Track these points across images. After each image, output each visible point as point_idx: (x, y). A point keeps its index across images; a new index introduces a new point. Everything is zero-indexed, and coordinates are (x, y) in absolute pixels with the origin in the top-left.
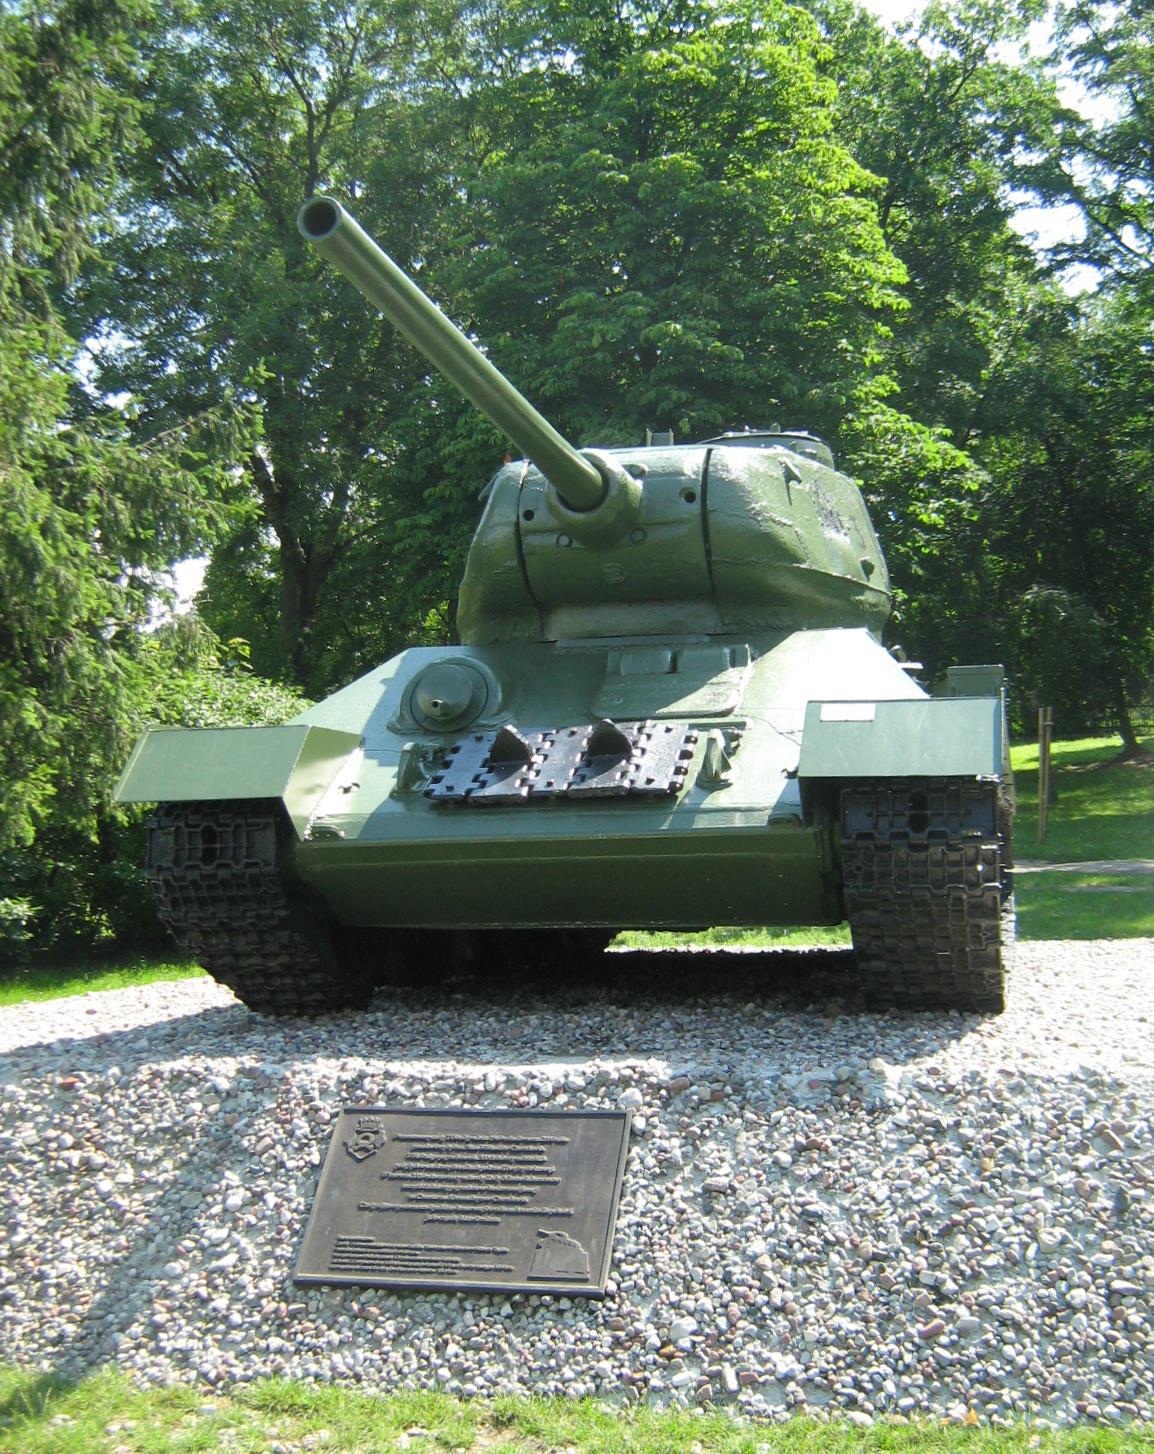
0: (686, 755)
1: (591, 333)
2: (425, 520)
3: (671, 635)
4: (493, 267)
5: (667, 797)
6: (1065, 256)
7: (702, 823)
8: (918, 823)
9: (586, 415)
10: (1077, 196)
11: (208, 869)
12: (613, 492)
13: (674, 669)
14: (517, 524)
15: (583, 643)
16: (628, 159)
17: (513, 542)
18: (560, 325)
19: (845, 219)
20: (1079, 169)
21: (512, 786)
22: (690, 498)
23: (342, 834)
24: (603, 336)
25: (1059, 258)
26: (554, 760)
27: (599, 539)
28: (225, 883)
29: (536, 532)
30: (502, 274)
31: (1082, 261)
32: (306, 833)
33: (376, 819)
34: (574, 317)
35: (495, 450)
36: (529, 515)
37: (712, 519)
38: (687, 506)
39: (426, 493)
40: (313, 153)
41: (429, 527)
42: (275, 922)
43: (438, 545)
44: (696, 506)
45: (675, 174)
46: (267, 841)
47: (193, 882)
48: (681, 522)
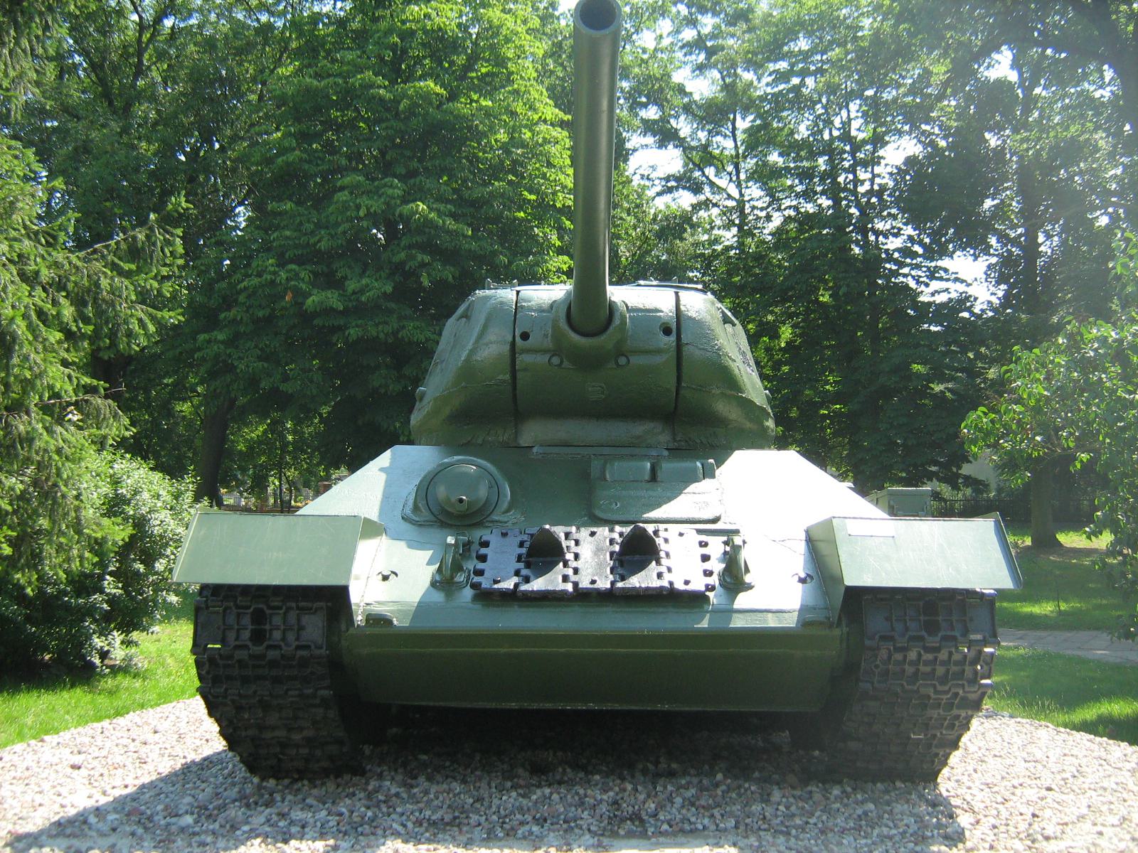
0: (705, 558)
1: (358, 207)
2: (221, 337)
3: (632, 448)
4: (283, 151)
5: (696, 600)
6: (673, 183)
7: (738, 622)
8: (932, 628)
9: (350, 267)
10: (681, 143)
11: (258, 650)
12: (617, 322)
13: (654, 478)
14: (513, 344)
15: (556, 450)
16: (393, 82)
17: (508, 360)
18: (335, 198)
19: (546, 141)
20: (684, 126)
21: (550, 582)
22: (667, 331)
23: (395, 622)
24: (368, 209)
25: (669, 185)
26: (589, 557)
27: (588, 363)
28: (273, 664)
29: (528, 351)
30: (291, 157)
31: (684, 188)
32: (359, 619)
33: (422, 608)
34: (346, 192)
35: (280, 288)
36: (525, 336)
37: (686, 350)
38: (666, 339)
39: (222, 316)
40: (140, 54)
41: (222, 342)
42: (318, 701)
43: (230, 356)
44: (673, 338)
45: (426, 96)
46: (314, 627)
47: (239, 661)
48: (659, 351)
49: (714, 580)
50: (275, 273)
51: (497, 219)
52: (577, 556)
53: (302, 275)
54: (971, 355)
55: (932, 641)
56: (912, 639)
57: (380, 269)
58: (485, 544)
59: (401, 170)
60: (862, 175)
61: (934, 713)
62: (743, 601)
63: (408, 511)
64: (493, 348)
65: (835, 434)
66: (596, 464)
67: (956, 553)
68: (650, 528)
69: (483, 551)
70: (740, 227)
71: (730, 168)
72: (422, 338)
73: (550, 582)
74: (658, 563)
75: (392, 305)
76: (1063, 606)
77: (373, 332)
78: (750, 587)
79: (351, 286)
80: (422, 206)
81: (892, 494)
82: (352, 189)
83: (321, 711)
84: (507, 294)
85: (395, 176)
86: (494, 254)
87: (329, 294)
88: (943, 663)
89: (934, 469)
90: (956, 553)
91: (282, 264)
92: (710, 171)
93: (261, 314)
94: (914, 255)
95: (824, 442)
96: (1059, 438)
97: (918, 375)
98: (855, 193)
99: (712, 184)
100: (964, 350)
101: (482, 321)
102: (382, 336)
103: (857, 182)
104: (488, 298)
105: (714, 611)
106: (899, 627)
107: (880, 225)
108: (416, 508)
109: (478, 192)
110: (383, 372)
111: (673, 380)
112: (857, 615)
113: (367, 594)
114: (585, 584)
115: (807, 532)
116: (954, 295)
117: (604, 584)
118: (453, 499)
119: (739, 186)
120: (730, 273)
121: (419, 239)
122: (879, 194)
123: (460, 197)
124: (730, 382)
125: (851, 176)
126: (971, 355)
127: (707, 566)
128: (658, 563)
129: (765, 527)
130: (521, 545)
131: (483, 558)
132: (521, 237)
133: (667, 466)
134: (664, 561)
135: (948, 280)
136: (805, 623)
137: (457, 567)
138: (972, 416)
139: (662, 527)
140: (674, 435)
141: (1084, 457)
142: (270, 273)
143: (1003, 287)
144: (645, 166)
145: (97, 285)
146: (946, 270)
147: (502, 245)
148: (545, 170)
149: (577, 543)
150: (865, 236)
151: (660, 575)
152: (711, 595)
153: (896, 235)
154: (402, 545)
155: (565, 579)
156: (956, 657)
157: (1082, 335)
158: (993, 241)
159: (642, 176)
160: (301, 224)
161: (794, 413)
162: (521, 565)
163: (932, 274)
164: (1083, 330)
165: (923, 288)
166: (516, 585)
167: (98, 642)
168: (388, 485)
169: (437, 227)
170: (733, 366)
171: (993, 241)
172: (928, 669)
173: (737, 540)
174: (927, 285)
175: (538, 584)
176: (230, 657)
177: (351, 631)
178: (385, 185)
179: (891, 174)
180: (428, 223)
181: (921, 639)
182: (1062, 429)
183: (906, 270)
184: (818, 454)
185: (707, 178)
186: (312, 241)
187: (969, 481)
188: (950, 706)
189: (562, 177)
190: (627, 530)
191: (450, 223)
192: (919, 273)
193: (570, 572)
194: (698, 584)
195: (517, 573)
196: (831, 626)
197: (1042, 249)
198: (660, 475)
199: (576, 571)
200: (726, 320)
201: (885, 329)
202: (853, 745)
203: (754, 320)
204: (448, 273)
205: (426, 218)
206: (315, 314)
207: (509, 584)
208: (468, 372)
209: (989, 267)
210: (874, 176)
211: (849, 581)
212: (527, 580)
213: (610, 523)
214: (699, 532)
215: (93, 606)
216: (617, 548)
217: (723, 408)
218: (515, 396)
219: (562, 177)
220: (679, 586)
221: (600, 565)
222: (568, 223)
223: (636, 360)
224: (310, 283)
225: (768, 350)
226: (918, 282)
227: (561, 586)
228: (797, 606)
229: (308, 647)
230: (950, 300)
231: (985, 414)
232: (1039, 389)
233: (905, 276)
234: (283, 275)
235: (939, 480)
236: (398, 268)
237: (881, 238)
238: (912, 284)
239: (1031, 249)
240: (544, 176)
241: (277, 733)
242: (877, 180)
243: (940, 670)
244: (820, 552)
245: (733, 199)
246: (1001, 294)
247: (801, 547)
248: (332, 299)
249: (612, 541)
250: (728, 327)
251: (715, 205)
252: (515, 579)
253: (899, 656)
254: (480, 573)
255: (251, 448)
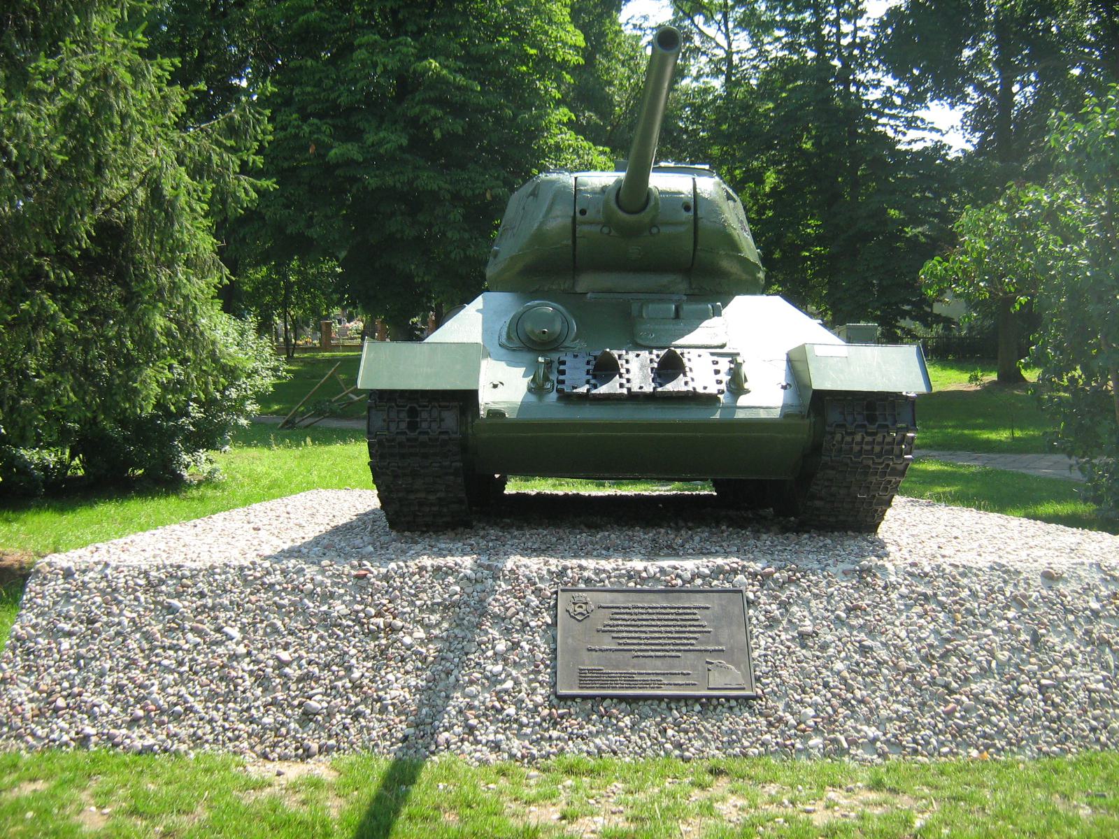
0: (717, 372)
1: (375, 65)
3: (660, 294)
5: (711, 400)
7: (740, 415)
8: (871, 419)
12: (652, 203)
15: (607, 295)
21: (611, 387)
22: (687, 208)
26: (637, 371)
27: (630, 232)
33: (524, 406)
34: (364, 51)
36: (583, 212)
37: (700, 223)
44: (691, 213)
48: (682, 224)
49: (723, 387)
50: (298, 127)
51: (501, 74)
52: (628, 371)
53: (324, 128)
54: (944, 201)
55: (872, 428)
56: (857, 426)
57: (395, 122)
58: (563, 363)
59: (411, 28)
60: (846, 27)
61: (873, 479)
62: (743, 401)
63: (504, 340)
64: (559, 220)
65: (815, 275)
66: (635, 307)
67: (891, 368)
68: (678, 351)
69: (562, 367)
70: (728, 79)
71: (719, 17)
72: (435, 187)
73: (611, 387)
74: (685, 375)
75: (407, 156)
76: (1018, 434)
77: (390, 181)
78: (748, 392)
79: (370, 138)
80: (434, 64)
81: (849, 328)
82: (371, 46)
83: (452, 478)
84: (568, 179)
85: (406, 34)
86: (502, 107)
87: (349, 146)
88: (879, 444)
89: (906, 308)
90: (891, 368)
91: (304, 118)
92: (699, 19)
93: (286, 165)
94: (892, 105)
95: (804, 282)
96: (1002, 283)
97: (894, 221)
98: (838, 44)
99: (701, 33)
100: (938, 196)
101: (548, 202)
102: (398, 185)
103: (840, 35)
104: (552, 182)
105: (724, 408)
106: (849, 418)
107: (861, 77)
108: (509, 338)
109: (484, 49)
110: (399, 218)
111: (691, 247)
112: (821, 409)
113: (488, 399)
114: (635, 389)
115: (788, 354)
116: (929, 144)
117: (649, 389)
118: (537, 332)
119: (727, 36)
120: (718, 122)
121: (432, 95)
122: (862, 46)
123: (468, 53)
124: (732, 244)
125: (834, 30)
126: (944, 201)
127: (719, 377)
128: (685, 375)
129: (759, 349)
130: (588, 363)
131: (563, 372)
132: (524, 90)
133: (687, 308)
134: (688, 374)
135: (924, 129)
136: (785, 415)
137: (546, 379)
138: (929, 264)
139: (686, 351)
140: (690, 284)
141: (1023, 299)
142: (294, 127)
143: (978, 134)
144: (637, 16)
145: (209, 159)
146: (923, 120)
147: (506, 98)
148: (547, 27)
149: (627, 362)
150: (847, 87)
151: (686, 383)
152: (721, 396)
153: (877, 83)
154: (503, 364)
155: (621, 386)
156: (888, 439)
157: (1019, 198)
158: (969, 90)
159: (635, 26)
160: (320, 80)
161: (777, 255)
162: (589, 377)
163: (911, 124)
164: (1020, 194)
165: (900, 137)
166: (588, 390)
167: (186, 458)
168: (484, 322)
169: (447, 82)
170: (735, 233)
171: (969, 90)
172: (869, 448)
173: (739, 360)
174: (904, 134)
175: (603, 389)
176: (393, 440)
177: (477, 421)
178: (399, 43)
179: (873, 27)
180: (440, 79)
181: (864, 426)
182: (1004, 276)
183: (883, 120)
184: (797, 298)
185: (697, 26)
186: (332, 96)
187: (938, 319)
188: (884, 474)
189: (562, 34)
190: (662, 353)
191: (461, 80)
192: (898, 123)
193: (624, 381)
194: (713, 389)
195: (588, 382)
196: (803, 417)
197: (1017, 98)
198: (682, 314)
199: (628, 380)
200: (729, 197)
201: (863, 176)
202: (818, 503)
203: (740, 168)
204: (458, 127)
205: (438, 74)
206: (338, 165)
207: (583, 389)
208: (539, 237)
209: (965, 115)
210: (856, 29)
211: (816, 386)
212: (595, 387)
213: (650, 349)
214: (712, 354)
215: (182, 428)
216: (656, 365)
217: (726, 264)
218: (574, 255)
219: (562, 34)
220: (700, 390)
221: (645, 377)
222: (568, 77)
223: (664, 230)
224: (331, 136)
225: (753, 195)
226: (896, 131)
227: (620, 391)
228: (780, 403)
229: (446, 433)
230: (926, 148)
231: (940, 263)
232: (981, 244)
233: (884, 125)
234: (306, 128)
235: (913, 318)
236: (414, 122)
237: (861, 89)
238: (890, 133)
239: (1007, 96)
240: (546, 33)
241: (419, 495)
242: (860, 34)
243: (877, 449)
244: (796, 366)
245: (722, 48)
246: (976, 141)
247: (784, 365)
248: (352, 150)
249: (652, 361)
250: (731, 203)
251: (704, 53)
252: (587, 386)
253: (848, 439)
254: (562, 382)
255: (256, 289)
